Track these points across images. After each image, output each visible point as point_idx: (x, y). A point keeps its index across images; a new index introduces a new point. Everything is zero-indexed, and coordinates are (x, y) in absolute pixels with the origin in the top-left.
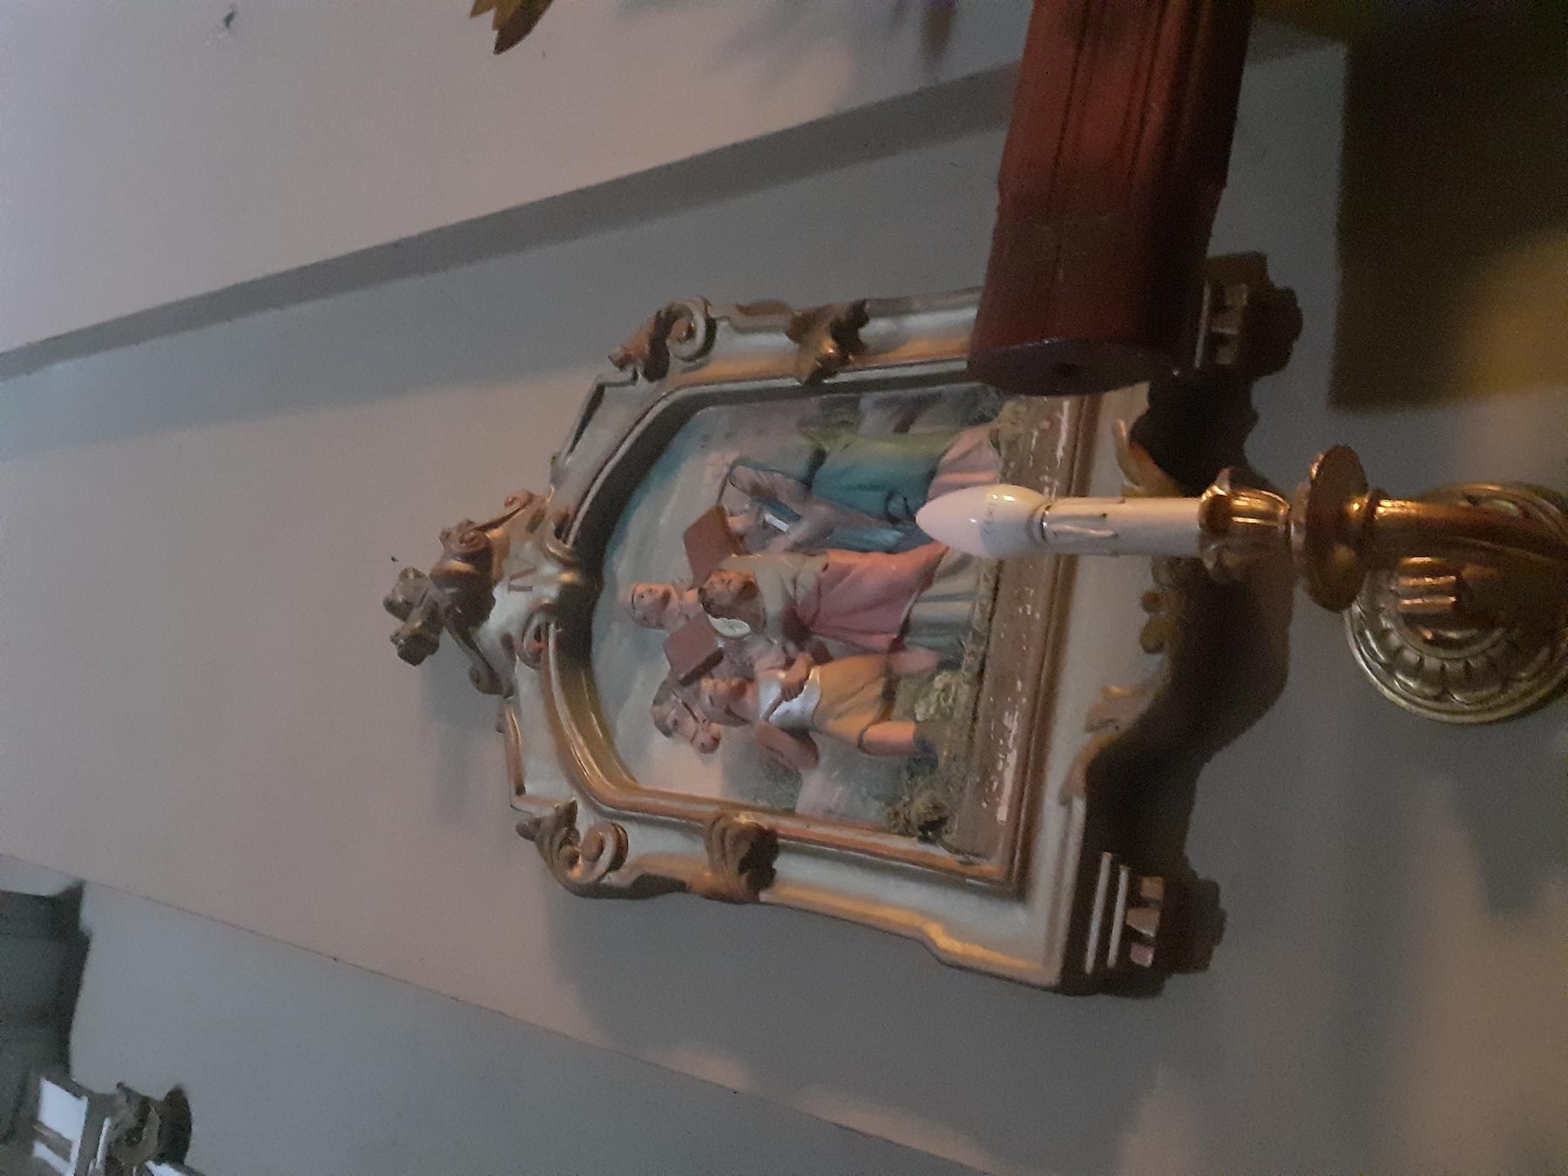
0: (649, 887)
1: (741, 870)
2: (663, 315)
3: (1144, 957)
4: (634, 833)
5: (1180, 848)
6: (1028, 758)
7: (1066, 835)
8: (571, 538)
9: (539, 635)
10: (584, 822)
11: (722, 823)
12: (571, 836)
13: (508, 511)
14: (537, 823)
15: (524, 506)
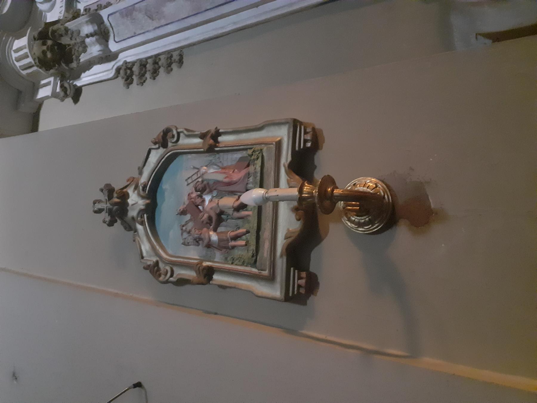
0: (182, 282)
1: (205, 277)
2: (165, 130)
3: (302, 291)
4: (175, 269)
5: (313, 173)
6: (272, 232)
7: (282, 265)
8: (147, 192)
9: (142, 217)
10: (161, 265)
11: (199, 265)
12: (159, 269)
13: (128, 183)
14: (149, 266)
15: (132, 181)
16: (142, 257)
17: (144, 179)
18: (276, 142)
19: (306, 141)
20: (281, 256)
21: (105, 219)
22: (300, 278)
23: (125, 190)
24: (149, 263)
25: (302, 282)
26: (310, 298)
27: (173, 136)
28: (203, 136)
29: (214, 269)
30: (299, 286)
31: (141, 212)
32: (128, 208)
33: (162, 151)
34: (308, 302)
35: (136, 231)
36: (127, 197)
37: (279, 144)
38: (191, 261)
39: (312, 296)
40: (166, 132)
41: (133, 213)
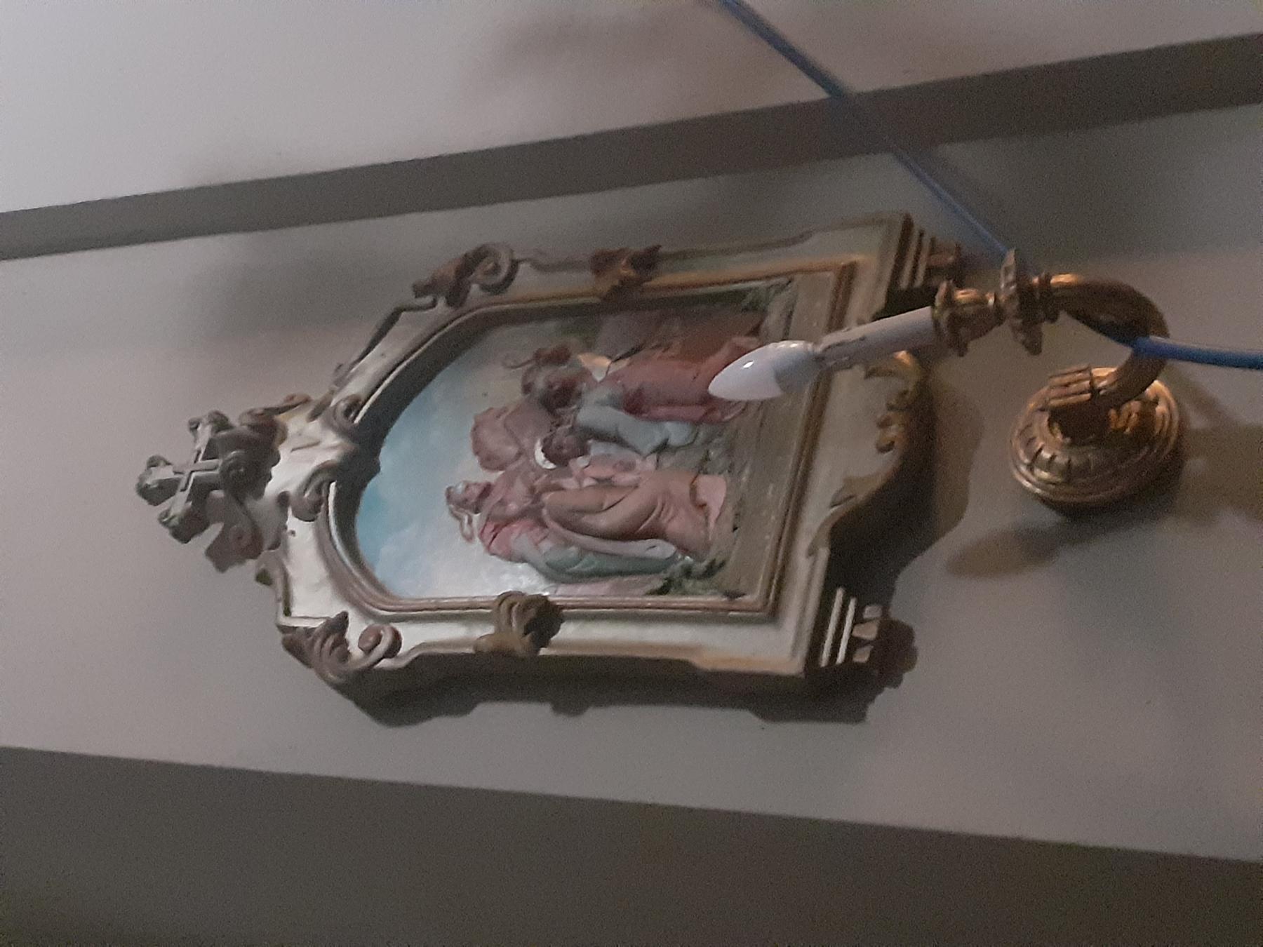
13: (290, 404)
17: (355, 387)
27: (496, 269)
34: (873, 710)
36: (279, 436)
40: (469, 264)
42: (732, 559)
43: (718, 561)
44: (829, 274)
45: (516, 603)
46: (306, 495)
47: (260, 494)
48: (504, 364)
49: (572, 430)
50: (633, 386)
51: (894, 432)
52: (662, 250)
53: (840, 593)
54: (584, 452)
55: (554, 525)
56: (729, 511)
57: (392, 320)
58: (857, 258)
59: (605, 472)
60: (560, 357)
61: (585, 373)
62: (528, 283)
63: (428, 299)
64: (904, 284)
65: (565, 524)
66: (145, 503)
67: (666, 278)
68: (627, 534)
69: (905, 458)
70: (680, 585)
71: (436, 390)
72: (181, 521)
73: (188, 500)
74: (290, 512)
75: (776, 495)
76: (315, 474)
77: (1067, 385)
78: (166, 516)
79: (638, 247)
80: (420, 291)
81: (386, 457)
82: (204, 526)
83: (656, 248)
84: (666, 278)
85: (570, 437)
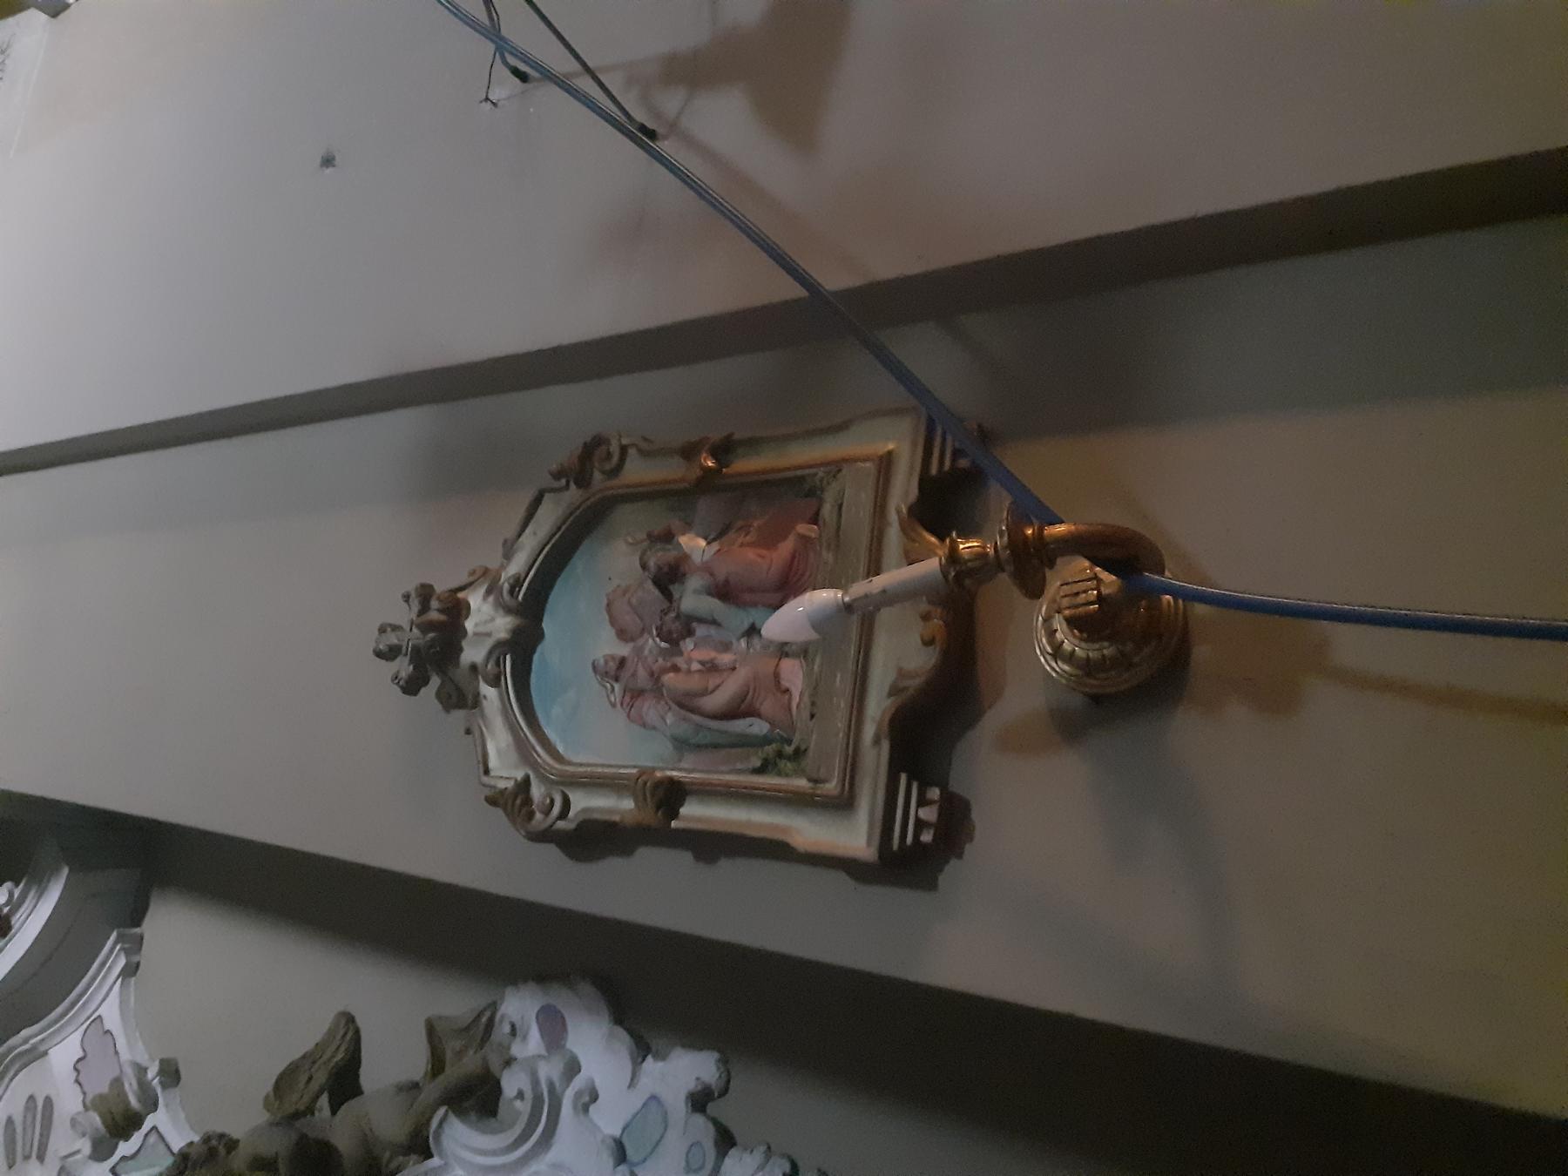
1: (658, 809)
8: (520, 598)
10: (537, 791)
12: (528, 801)
13: (472, 579)
16: (487, 772)
17: (516, 566)
18: (881, 458)
19: (957, 454)
20: (877, 741)
21: (398, 672)
22: (922, 802)
23: (460, 595)
24: (502, 785)
25: (929, 814)
26: (948, 868)
27: (609, 455)
28: (689, 452)
29: (687, 787)
30: (920, 825)
31: (500, 649)
32: (464, 644)
33: (573, 494)
34: (943, 879)
35: (476, 702)
36: (464, 612)
37: (886, 464)
38: (622, 771)
39: (954, 862)
40: (592, 449)
41: (473, 653)
42: (812, 746)
43: (803, 748)
44: (868, 464)
45: (648, 780)
46: (489, 666)
47: (457, 663)
48: (626, 542)
49: (678, 617)
50: (721, 577)
51: (937, 622)
52: (736, 437)
53: (903, 778)
54: (690, 633)
55: (674, 707)
56: (806, 699)
57: (537, 502)
58: (891, 446)
59: (707, 654)
60: (668, 537)
61: (685, 558)
62: (637, 471)
63: (563, 481)
64: (934, 471)
65: (681, 705)
66: (383, 662)
67: (746, 464)
68: (731, 713)
69: (945, 654)
70: (776, 764)
71: (578, 563)
72: (407, 682)
73: (409, 665)
74: (480, 677)
75: (842, 682)
76: (490, 653)
77: (1077, 594)
78: (396, 678)
79: (716, 436)
80: (557, 476)
81: (547, 625)
82: (426, 682)
83: (729, 436)
84: (746, 464)
85: (677, 624)
